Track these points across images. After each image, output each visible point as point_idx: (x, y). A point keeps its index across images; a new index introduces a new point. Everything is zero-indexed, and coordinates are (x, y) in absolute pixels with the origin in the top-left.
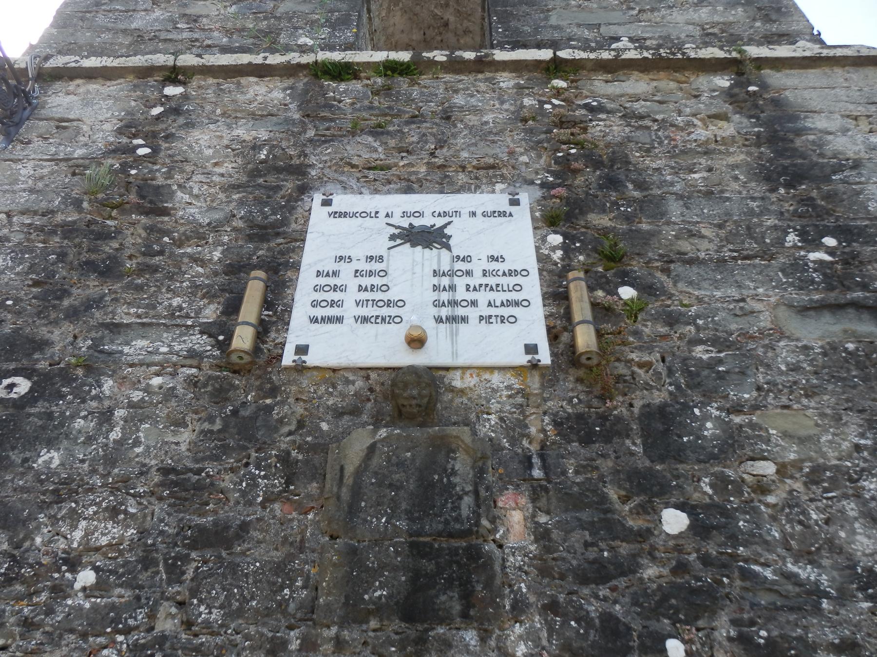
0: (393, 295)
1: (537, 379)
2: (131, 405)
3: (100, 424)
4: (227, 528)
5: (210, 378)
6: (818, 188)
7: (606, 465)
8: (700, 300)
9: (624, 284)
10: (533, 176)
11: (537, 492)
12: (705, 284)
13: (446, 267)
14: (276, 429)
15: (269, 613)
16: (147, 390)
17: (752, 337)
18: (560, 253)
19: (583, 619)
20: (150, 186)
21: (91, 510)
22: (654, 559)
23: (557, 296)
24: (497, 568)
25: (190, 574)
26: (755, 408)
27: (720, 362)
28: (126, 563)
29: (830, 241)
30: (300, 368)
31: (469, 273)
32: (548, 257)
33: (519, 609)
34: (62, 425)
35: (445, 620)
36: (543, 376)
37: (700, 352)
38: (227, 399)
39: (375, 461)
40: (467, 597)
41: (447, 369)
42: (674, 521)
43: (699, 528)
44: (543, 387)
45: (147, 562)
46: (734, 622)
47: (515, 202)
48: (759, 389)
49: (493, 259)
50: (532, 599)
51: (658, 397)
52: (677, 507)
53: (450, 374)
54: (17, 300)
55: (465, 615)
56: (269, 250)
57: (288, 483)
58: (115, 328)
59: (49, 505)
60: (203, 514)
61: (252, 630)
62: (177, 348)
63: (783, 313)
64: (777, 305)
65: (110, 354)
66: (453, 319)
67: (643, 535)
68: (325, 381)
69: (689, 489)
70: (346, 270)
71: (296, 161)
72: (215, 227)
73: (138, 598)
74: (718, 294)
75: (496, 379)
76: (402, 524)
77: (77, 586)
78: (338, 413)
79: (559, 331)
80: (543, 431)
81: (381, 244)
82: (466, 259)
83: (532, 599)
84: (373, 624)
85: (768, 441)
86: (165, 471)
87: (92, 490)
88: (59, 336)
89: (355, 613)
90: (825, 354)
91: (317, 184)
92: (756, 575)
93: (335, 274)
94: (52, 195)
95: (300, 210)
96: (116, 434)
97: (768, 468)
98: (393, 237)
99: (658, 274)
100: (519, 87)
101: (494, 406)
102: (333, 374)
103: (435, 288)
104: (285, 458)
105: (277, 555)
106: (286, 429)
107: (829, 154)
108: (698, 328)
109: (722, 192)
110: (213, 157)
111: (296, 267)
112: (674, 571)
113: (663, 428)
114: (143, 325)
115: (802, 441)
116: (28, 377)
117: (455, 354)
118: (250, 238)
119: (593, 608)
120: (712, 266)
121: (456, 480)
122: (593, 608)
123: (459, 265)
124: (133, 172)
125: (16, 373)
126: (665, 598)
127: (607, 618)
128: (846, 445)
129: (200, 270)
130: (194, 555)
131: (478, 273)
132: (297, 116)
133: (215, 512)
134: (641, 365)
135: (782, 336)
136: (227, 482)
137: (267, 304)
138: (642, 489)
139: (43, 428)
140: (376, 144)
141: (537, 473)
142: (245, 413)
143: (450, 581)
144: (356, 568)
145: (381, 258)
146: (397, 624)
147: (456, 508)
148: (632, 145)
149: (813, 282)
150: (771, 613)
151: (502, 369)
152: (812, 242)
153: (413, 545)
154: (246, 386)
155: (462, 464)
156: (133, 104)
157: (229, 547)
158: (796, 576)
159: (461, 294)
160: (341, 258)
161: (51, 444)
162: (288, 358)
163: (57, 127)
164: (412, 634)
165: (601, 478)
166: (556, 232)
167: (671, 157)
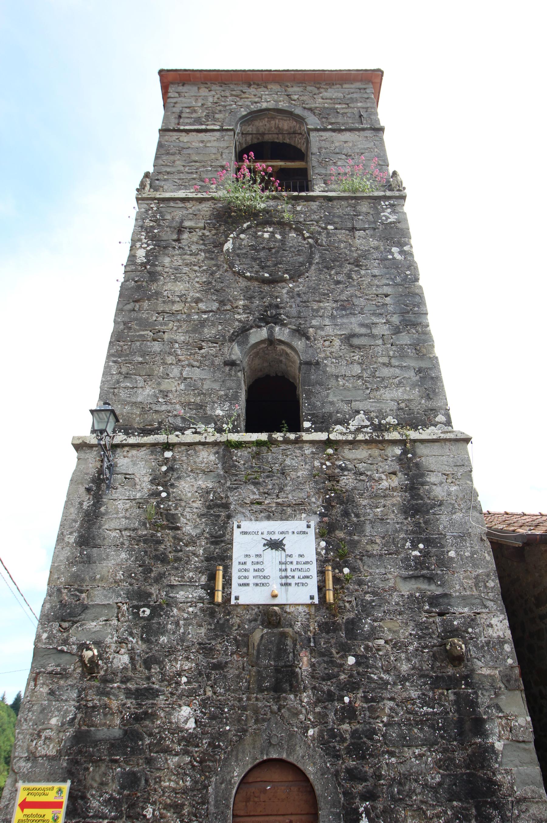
0: (265, 573)
1: (313, 608)
2: (185, 619)
3: (176, 627)
4: (221, 663)
5: (208, 608)
6: (424, 517)
7: (333, 641)
8: (371, 574)
9: (346, 567)
10: (316, 509)
11: (312, 651)
12: (373, 567)
13: (283, 560)
14: (231, 628)
15: (237, 690)
16: (188, 613)
17: (386, 591)
18: (324, 551)
19: (323, 692)
20: (170, 514)
21: (181, 657)
22: (344, 673)
23: (322, 573)
24: (300, 676)
25: (213, 678)
26: (382, 620)
27: (373, 601)
28: (194, 675)
29: (421, 546)
30: (237, 605)
31: (291, 563)
32: (320, 553)
33: (305, 688)
34: (164, 627)
35: (285, 692)
36: (315, 607)
37: (368, 597)
38: (215, 616)
39: (263, 641)
40: (291, 685)
41: (284, 605)
42: (351, 660)
43: (358, 663)
44: (315, 611)
45: (200, 674)
46: (364, 692)
47: (309, 527)
48: (384, 612)
49: (301, 556)
50: (309, 685)
51: (352, 615)
52: (353, 656)
53: (286, 607)
54: (135, 574)
55: (290, 690)
56: (219, 555)
57: (237, 648)
58: (172, 586)
59: (168, 656)
60: (213, 659)
61: (233, 695)
62: (195, 595)
63: (398, 580)
64: (397, 576)
65: (173, 598)
66: (286, 584)
67: (341, 665)
68: (245, 609)
69: (357, 649)
70: (249, 561)
71: (224, 501)
72: (198, 537)
73: (200, 686)
74: (377, 571)
75: (301, 609)
76: (272, 663)
77: (183, 682)
78: (250, 621)
79: (321, 589)
80: (315, 629)
81: (260, 548)
82: (290, 556)
83: (309, 685)
84: (266, 693)
85: (383, 632)
86: (200, 644)
87: (179, 651)
88: (154, 590)
89: (261, 690)
90: (408, 598)
91: (234, 514)
92: (372, 678)
93: (245, 563)
94: (134, 520)
95: (229, 528)
96: (182, 630)
97: (382, 642)
98: (264, 545)
99: (358, 561)
100: (313, 453)
101: (300, 619)
102: (247, 607)
103: (280, 570)
104: (235, 639)
105: (237, 672)
106: (234, 628)
107: (432, 497)
108: (369, 587)
109: (387, 519)
110: (191, 498)
111: (231, 558)
112: (349, 677)
113: (352, 626)
114: (181, 585)
115: (394, 632)
116: (149, 608)
117: (287, 599)
118: (212, 543)
119: (325, 688)
120: (377, 557)
121: (288, 647)
122: (325, 688)
123: (289, 559)
124: (162, 506)
125: (144, 606)
126: (345, 685)
127: (329, 691)
128: (407, 634)
129: (196, 559)
130: (213, 672)
131: (295, 563)
132: (222, 473)
133: (217, 658)
134: (348, 602)
135: (396, 590)
136: (219, 647)
137: (224, 577)
138: (343, 650)
139: (159, 628)
140: (255, 490)
141: (312, 644)
142: (221, 622)
143: (286, 680)
144: (260, 678)
145: (261, 555)
146: (272, 693)
147: (288, 657)
148: (356, 492)
149: (411, 566)
150: (373, 690)
151: (302, 605)
152: (414, 547)
153: (276, 670)
154: (218, 612)
155: (289, 642)
156: (153, 464)
157: (223, 670)
158: (383, 678)
159: (289, 573)
160: (247, 556)
161: (163, 634)
162: (233, 602)
163: (126, 478)
164: (276, 696)
165: (331, 646)
166: (323, 540)
167: (371, 498)
